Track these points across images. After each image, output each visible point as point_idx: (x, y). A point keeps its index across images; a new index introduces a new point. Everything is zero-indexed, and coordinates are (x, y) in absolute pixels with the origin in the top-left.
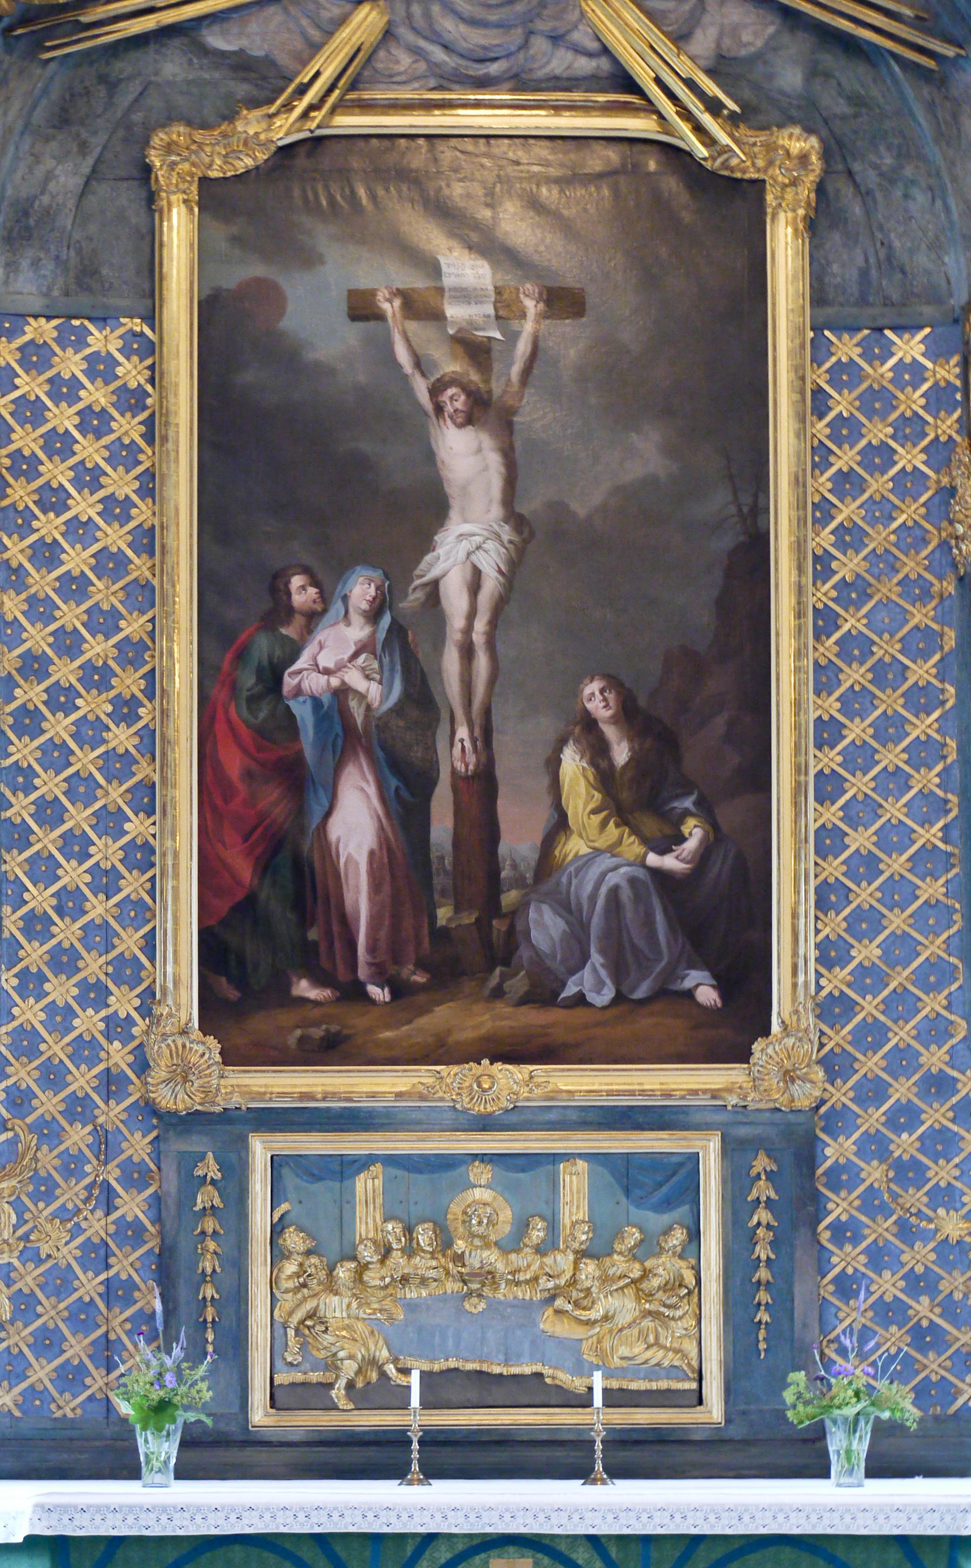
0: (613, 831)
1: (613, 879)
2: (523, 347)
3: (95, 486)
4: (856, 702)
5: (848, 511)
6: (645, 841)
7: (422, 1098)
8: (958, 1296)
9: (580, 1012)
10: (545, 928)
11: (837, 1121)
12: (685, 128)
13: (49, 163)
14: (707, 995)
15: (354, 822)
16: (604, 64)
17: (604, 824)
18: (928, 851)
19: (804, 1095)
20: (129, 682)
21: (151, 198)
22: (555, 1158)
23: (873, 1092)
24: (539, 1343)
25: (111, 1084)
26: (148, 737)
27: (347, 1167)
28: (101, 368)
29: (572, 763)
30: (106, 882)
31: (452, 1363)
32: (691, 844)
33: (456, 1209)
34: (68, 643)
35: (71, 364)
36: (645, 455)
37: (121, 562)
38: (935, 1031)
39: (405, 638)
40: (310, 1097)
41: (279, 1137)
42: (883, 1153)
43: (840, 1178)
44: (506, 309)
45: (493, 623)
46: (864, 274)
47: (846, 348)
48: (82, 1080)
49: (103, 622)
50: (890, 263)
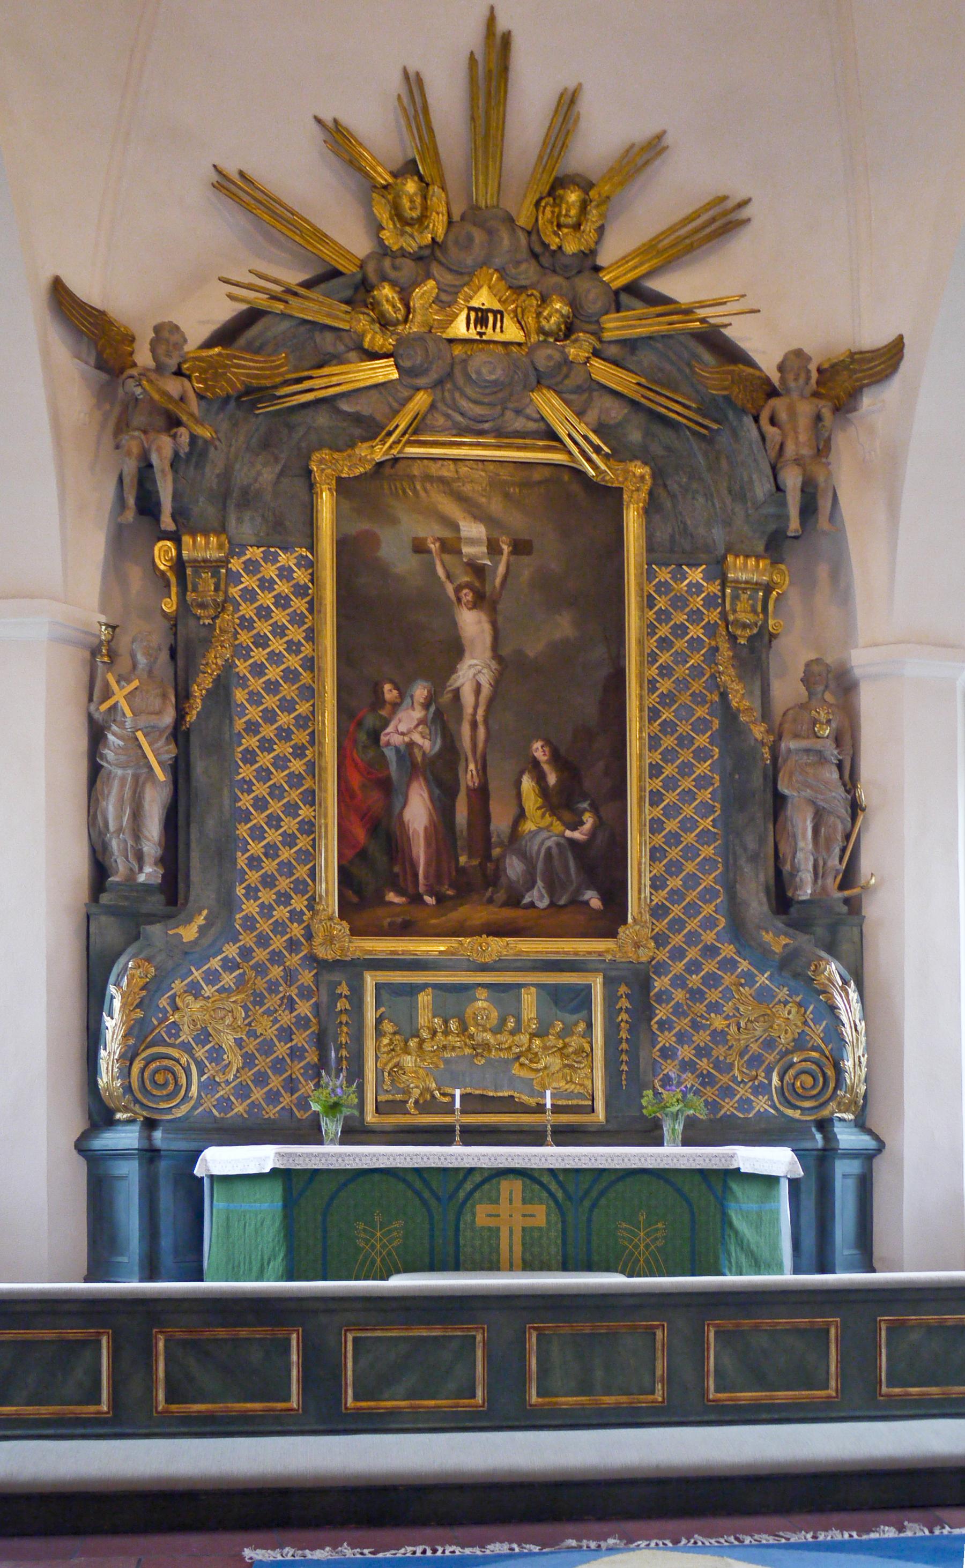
0: (548, 819)
1: (548, 843)
2: (501, 569)
3: (282, 635)
8: (721, 1058)
10: (514, 868)
11: (661, 968)
13: (259, 467)
14: (596, 903)
15: (417, 811)
16: (542, 425)
17: (543, 815)
19: (644, 955)
25: (293, 945)
27: (413, 990)
28: (285, 574)
29: (527, 784)
33: (469, 1011)
39: (443, 716)
42: (683, 985)
43: (663, 997)
44: (493, 548)
46: (672, 537)
47: (664, 574)
48: (278, 943)
50: (685, 531)
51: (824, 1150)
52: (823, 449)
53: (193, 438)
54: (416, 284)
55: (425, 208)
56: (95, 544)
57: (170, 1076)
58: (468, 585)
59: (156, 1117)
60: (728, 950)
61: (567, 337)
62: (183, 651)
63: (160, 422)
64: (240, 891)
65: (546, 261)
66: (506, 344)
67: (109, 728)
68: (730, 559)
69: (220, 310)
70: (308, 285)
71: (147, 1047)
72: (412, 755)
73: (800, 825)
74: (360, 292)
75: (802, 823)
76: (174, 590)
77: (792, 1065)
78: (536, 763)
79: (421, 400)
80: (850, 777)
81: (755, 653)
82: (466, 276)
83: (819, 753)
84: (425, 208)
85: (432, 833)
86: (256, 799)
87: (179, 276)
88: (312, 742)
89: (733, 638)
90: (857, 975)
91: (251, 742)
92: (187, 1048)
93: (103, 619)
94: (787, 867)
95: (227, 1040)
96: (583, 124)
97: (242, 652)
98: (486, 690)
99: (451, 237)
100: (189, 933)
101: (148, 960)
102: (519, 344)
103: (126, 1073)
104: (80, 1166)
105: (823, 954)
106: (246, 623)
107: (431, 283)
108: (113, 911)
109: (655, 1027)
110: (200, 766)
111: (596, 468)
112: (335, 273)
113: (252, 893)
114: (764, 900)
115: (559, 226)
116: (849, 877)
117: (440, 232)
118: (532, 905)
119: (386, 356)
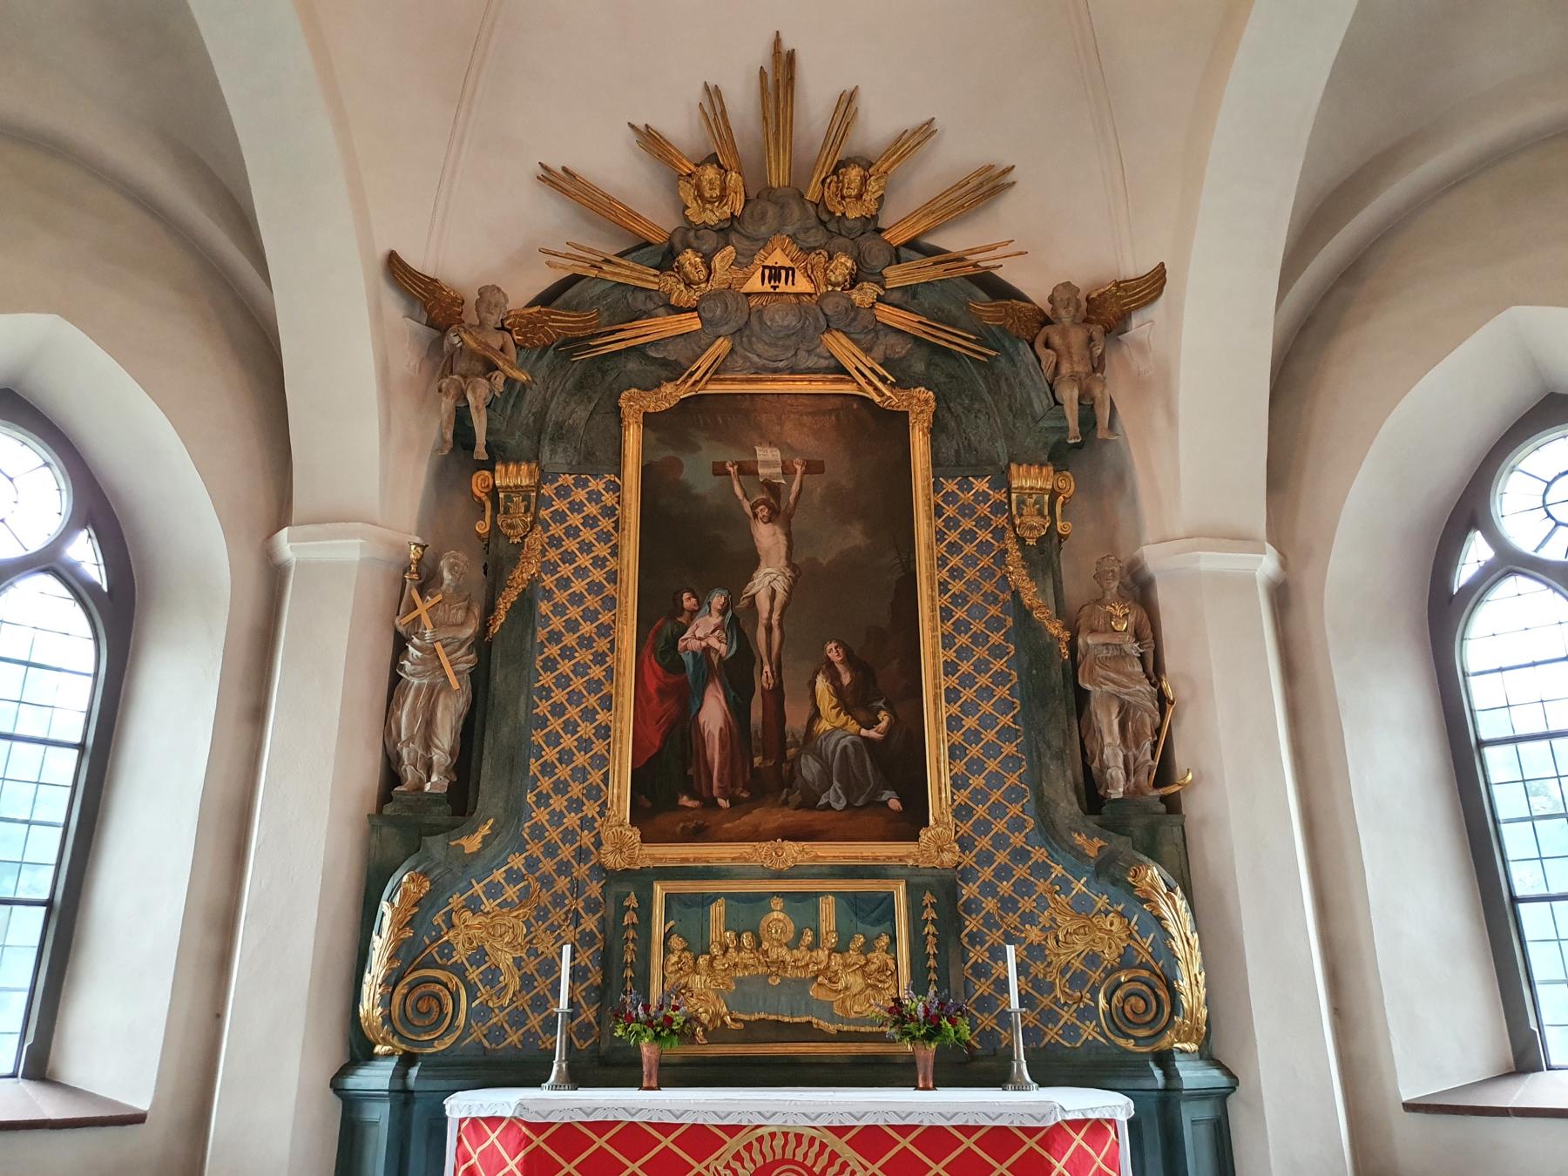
0: (843, 717)
1: (843, 742)
2: (795, 487)
3: (589, 551)
4: (964, 653)
5: (955, 561)
6: (859, 723)
7: (746, 860)
8: (1041, 976)
9: (829, 812)
10: (810, 768)
11: (967, 874)
12: (870, 389)
13: (573, 405)
14: (895, 804)
15: (713, 713)
16: (832, 362)
17: (838, 714)
18: (1006, 728)
19: (948, 858)
20: (602, 645)
21: (621, 421)
22: (817, 895)
23: (986, 858)
24: (809, 1004)
25: (582, 854)
26: (609, 671)
27: (707, 900)
28: (594, 497)
29: (822, 684)
30: (584, 745)
31: (762, 1015)
32: (883, 724)
33: (764, 924)
34: (572, 626)
35: (580, 495)
36: (855, 536)
37: (601, 587)
38: (1017, 825)
39: (739, 623)
40: (687, 860)
41: (669, 883)
42: (994, 894)
43: (971, 906)
44: (787, 470)
45: (782, 615)
46: (957, 452)
47: (951, 486)
48: (566, 852)
49: (590, 616)
50: (970, 447)
51: (1166, 1089)
52: (1098, 365)
53: (510, 382)
54: (716, 250)
55: (724, 188)
56: (415, 477)
57: (434, 1003)
58: (763, 502)
59: (416, 1050)
60: (1039, 854)
61: (852, 287)
62: (496, 561)
63: (479, 367)
64: (530, 798)
65: (832, 226)
66: (797, 295)
67: (409, 640)
68: (1013, 467)
69: (546, 279)
70: (621, 255)
71: (414, 970)
72: (709, 661)
73: (1105, 721)
74: (667, 259)
75: (1108, 722)
76: (488, 513)
77: (1119, 985)
78: (830, 664)
79: (722, 346)
80: (1154, 669)
81: (1044, 555)
82: (764, 243)
83: (1119, 647)
84: (724, 188)
85: (727, 735)
86: (554, 706)
87: (498, 244)
88: (612, 650)
89: (1021, 540)
90: (1183, 879)
91: (553, 650)
92: (459, 971)
93: (418, 540)
94: (1096, 765)
95: (505, 959)
96: (861, 113)
97: (550, 567)
98: (781, 596)
99: (748, 211)
100: (472, 844)
101: (425, 874)
102: (810, 295)
103: (386, 1001)
104: (337, 1105)
105: (1145, 859)
106: (555, 542)
107: (730, 248)
108: (393, 821)
109: (965, 941)
110: (498, 678)
111: (888, 397)
112: (648, 244)
113: (543, 800)
114: (1074, 799)
115: (843, 198)
116: (1165, 773)
117: (739, 207)
118: (828, 806)
119: (695, 310)
